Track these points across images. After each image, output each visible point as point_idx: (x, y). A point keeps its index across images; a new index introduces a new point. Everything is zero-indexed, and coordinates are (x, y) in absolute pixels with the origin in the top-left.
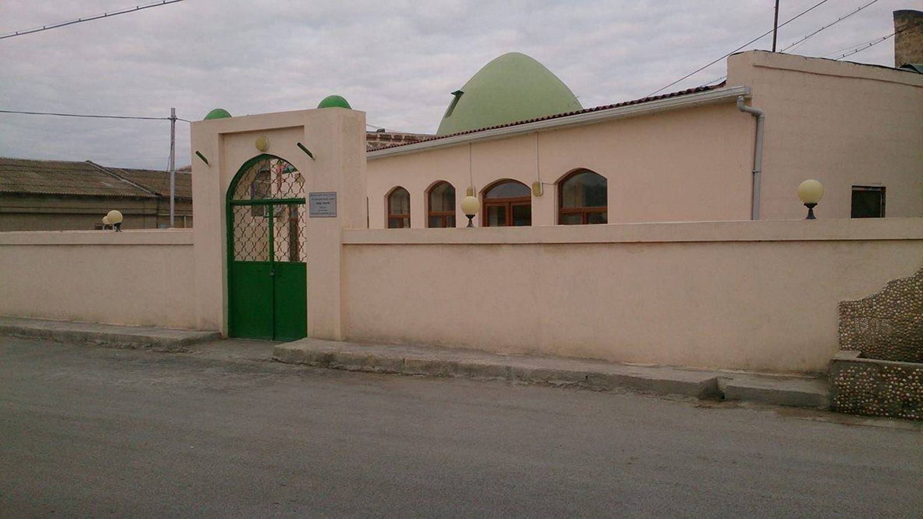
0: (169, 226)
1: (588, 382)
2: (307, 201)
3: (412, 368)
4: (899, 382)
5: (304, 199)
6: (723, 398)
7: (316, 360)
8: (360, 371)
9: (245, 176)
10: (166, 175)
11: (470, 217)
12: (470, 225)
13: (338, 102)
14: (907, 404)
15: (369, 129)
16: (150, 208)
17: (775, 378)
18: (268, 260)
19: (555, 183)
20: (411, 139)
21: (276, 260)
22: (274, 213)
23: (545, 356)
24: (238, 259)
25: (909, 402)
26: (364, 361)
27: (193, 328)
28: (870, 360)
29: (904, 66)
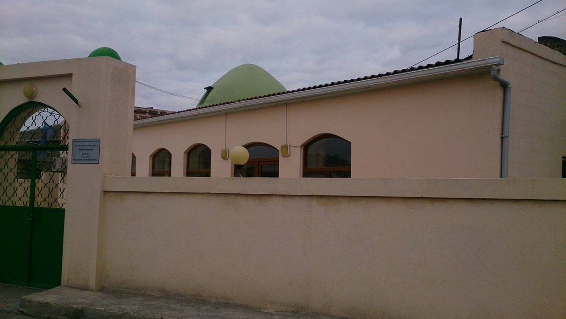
9: (12, 122)
13: (112, 54)
19: (301, 146)
21: (36, 205)
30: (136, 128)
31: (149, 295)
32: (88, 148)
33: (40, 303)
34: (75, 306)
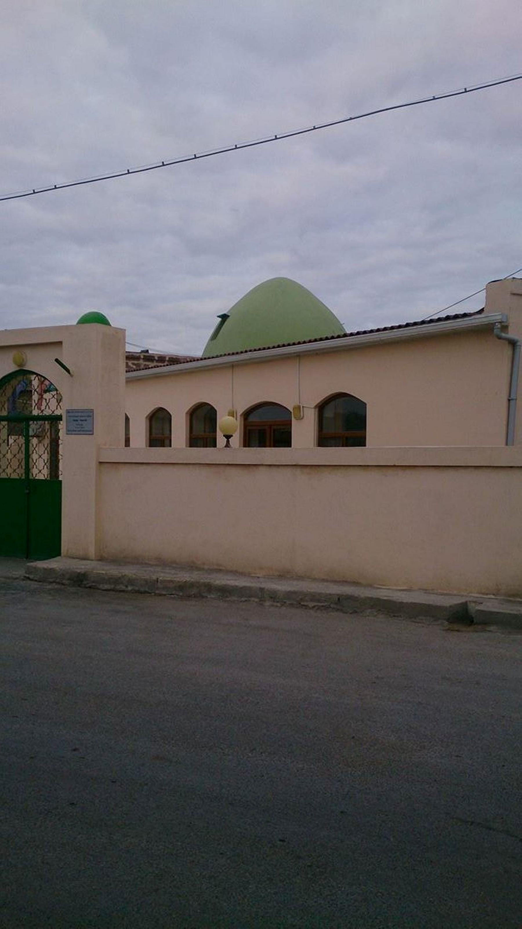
1: (342, 604)
2: (64, 418)
5: (61, 416)
6: (472, 622)
7: (69, 579)
11: (228, 437)
12: (228, 445)
13: (98, 319)
15: (129, 348)
18: (23, 477)
19: (316, 407)
21: (31, 477)
23: (300, 578)
26: (116, 580)
30: (129, 381)
31: (146, 564)
32: (82, 418)
33: (45, 569)
34: (79, 571)
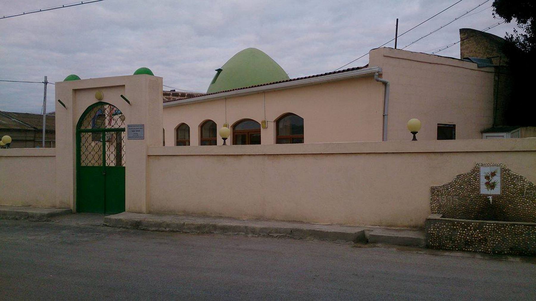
0: (42, 147)
1: (292, 234)
2: (126, 130)
3: (189, 229)
4: (463, 231)
8: (156, 231)
9: (88, 115)
10: (40, 117)
11: (225, 139)
12: (224, 144)
13: (146, 72)
14: (468, 243)
16: (30, 136)
17: (396, 230)
18: (102, 165)
20: (191, 96)
21: (107, 165)
22: (106, 139)
23: (268, 220)
24: (83, 164)
25: (469, 242)
26: (160, 225)
27: (54, 207)
28: (447, 219)
29: (464, 58)
34: (136, 220)
